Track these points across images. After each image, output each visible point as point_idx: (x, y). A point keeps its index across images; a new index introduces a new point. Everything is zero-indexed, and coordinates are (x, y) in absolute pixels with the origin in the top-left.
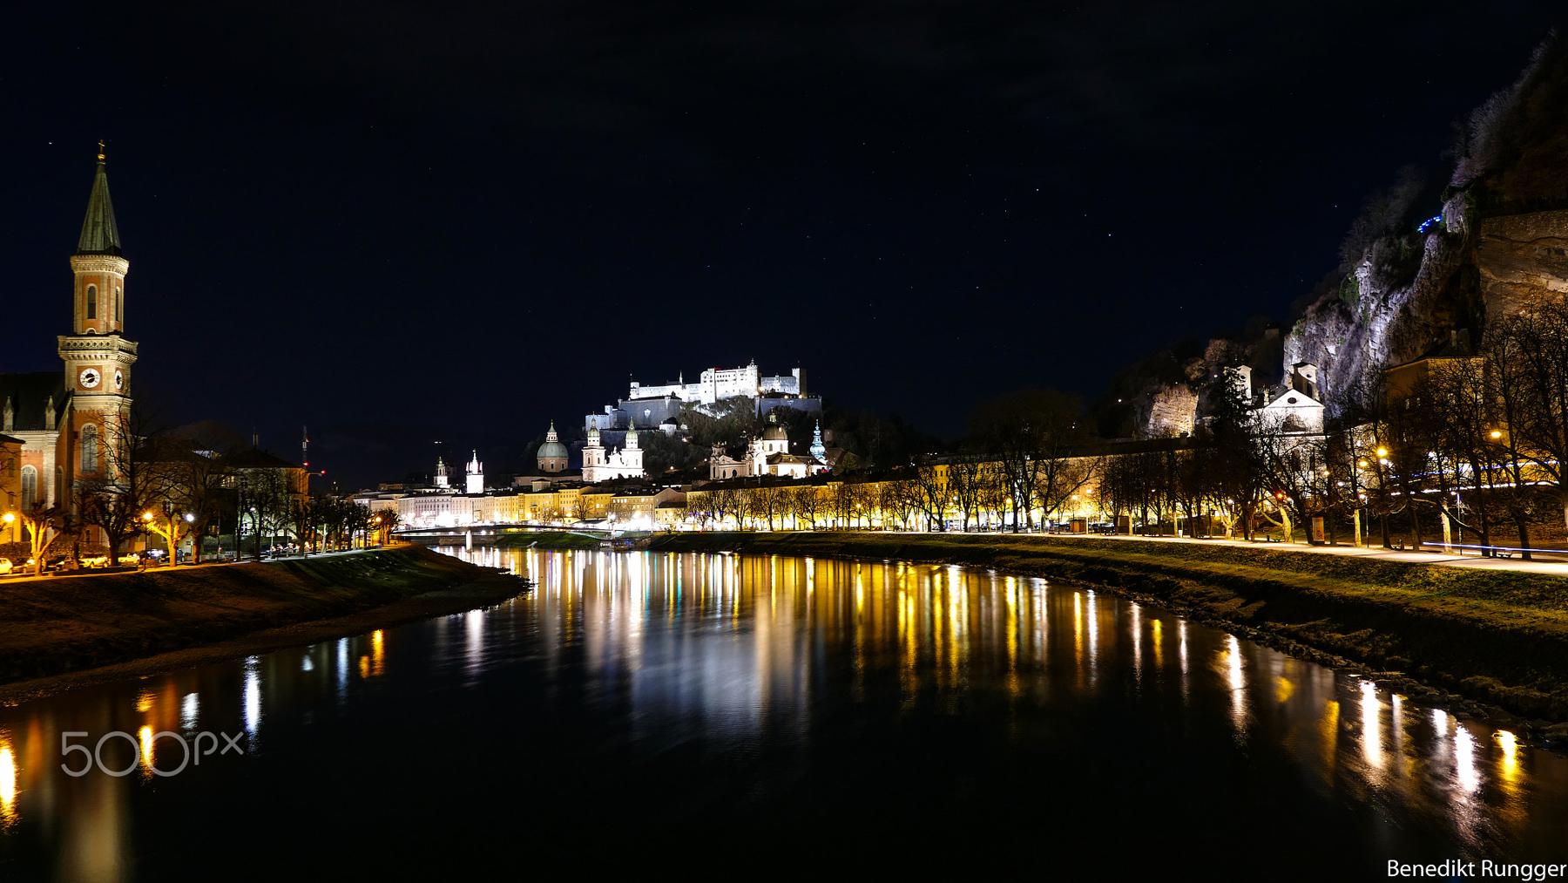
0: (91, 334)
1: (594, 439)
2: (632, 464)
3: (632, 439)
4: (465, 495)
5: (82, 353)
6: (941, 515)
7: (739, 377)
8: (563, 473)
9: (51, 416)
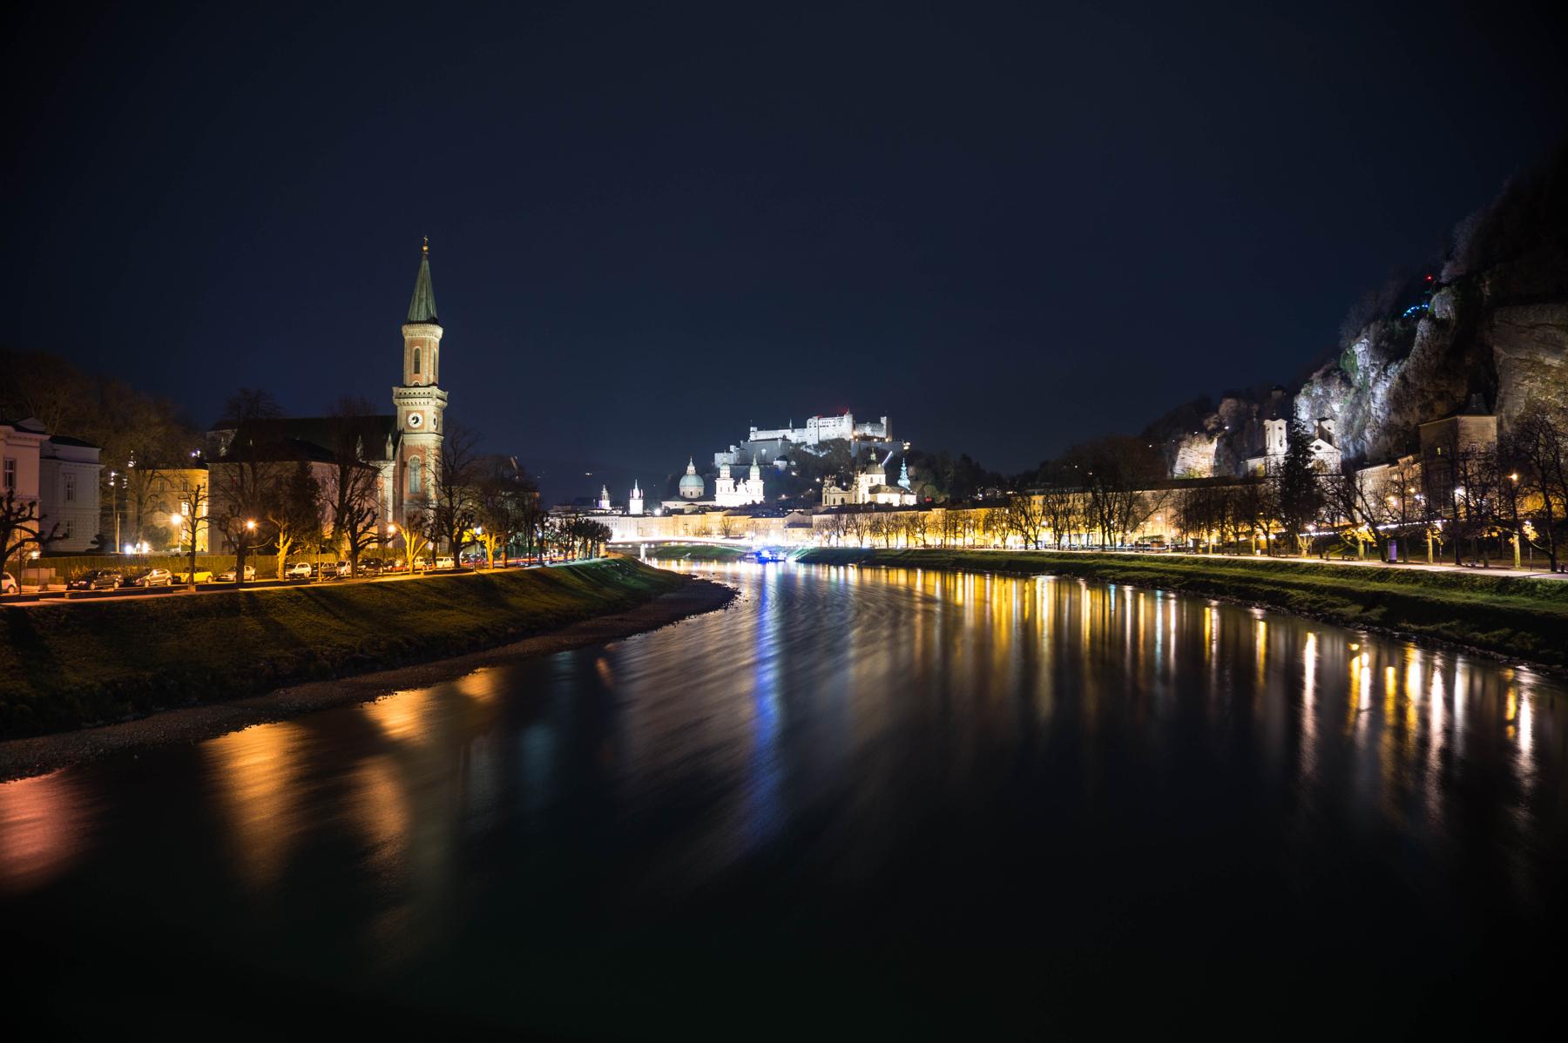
0: (417, 386)
1: (725, 472)
2: (755, 492)
3: (755, 472)
4: (628, 515)
5: (410, 401)
6: (1036, 537)
7: (837, 424)
8: (699, 499)
9: (390, 449)
